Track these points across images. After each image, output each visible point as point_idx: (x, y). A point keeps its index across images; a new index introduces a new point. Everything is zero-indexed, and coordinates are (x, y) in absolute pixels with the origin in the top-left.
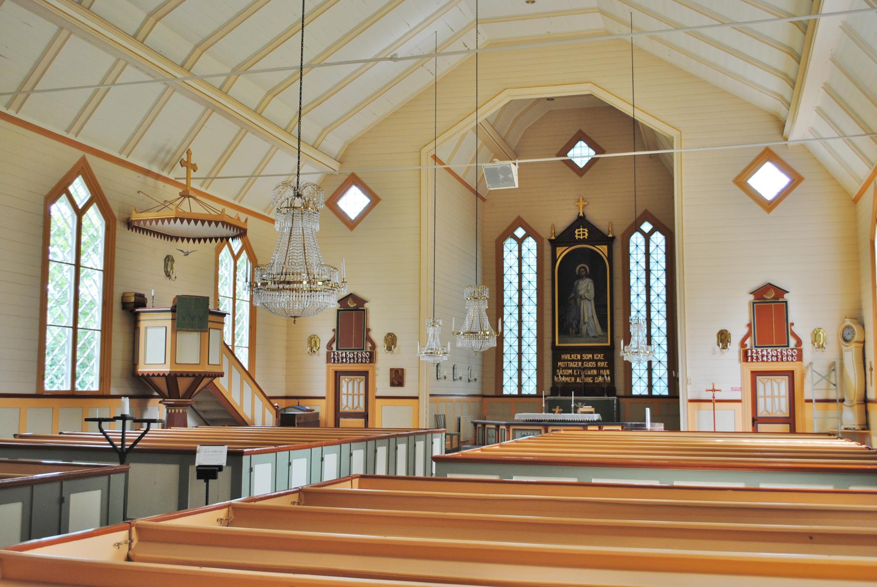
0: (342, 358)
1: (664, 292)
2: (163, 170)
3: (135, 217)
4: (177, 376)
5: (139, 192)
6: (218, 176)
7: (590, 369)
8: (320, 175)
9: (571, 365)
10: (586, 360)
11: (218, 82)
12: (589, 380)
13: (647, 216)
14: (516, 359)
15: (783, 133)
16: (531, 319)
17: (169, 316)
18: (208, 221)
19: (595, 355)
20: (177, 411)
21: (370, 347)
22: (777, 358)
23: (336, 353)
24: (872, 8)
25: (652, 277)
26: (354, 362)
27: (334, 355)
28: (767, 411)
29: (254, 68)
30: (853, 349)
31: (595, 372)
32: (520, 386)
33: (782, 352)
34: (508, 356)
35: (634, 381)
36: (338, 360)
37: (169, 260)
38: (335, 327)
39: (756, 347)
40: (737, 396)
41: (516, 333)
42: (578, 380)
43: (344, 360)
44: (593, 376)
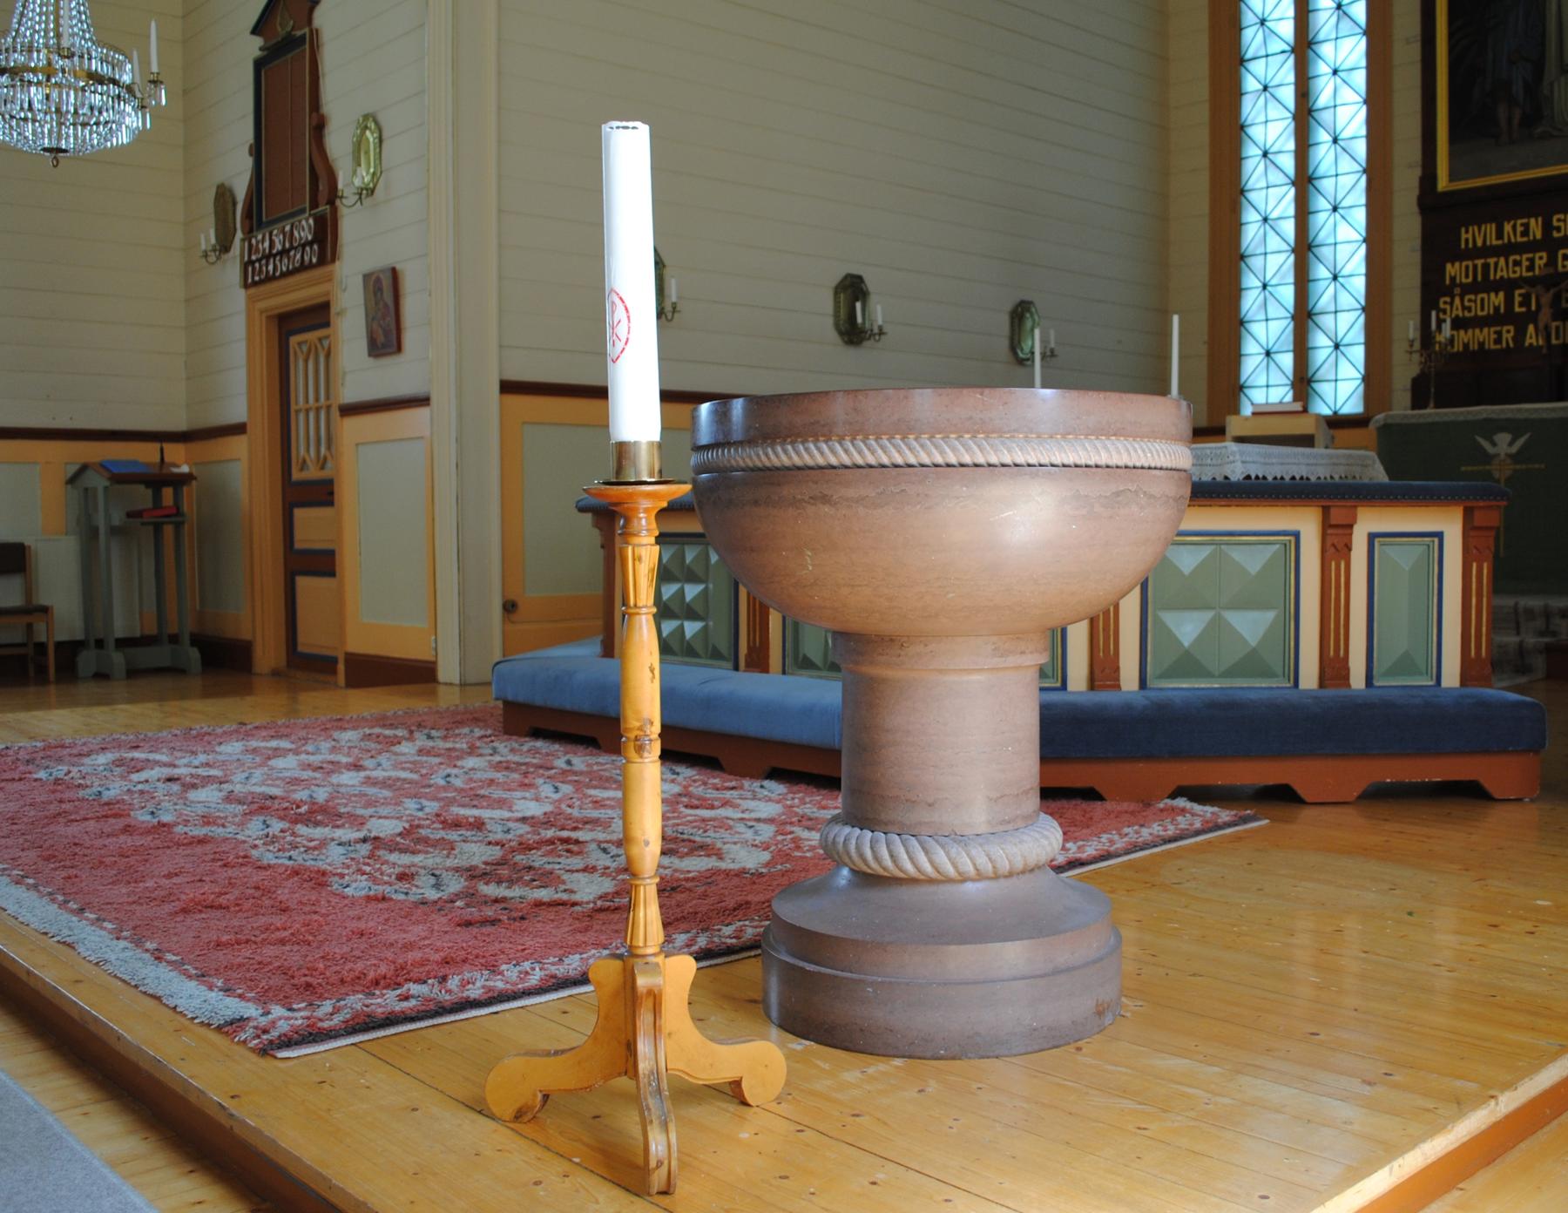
9: (1502, 269)
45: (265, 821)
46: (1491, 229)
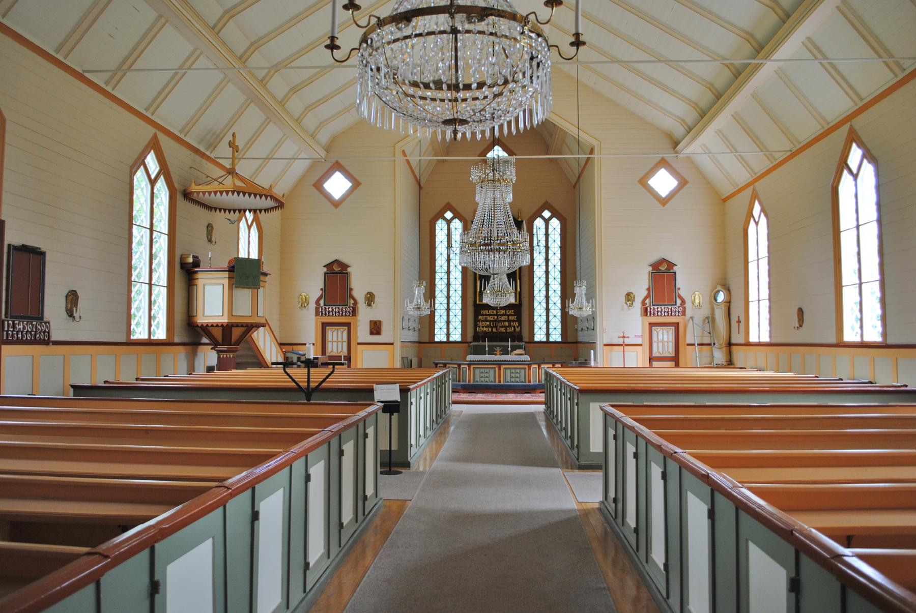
0: (329, 312)
1: (559, 264)
2: (207, 149)
3: (194, 188)
4: (234, 326)
5: (191, 167)
6: (244, 157)
7: (504, 321)
8: (310, 160)
9: (489, 318)
10: (500, 315)
11: (261, 74)
12: (503, 330)
13: (546, 206)
14: (445, 314)
15: (676, 147)
16: (457, 283)
17: (226, 275)
18: (254, 194)
19: (507, 311)
20: (228, 356)
21: (353, 304)
22: (339, 314)
23: (324, 308)
24: (815, 59)
25: (550, 252)
26: (339, 316)
27: (322, 309)
28: (659, 352)
29: (293, 64)
30: (723, 307)
31: (507, 324)
32: (448, 335)
33: (671, 309)
34: (439, 311)
35: (536, 330)
36: (325, 314)
37: (210, 227)
38: (322, 287)
39: (653, 305)
40: (639, 341)
41: (446, 293)
42: (494, 330)
43: (331, 314)
44: (506, 327)
45: (498, 118)
46: (487, 311)
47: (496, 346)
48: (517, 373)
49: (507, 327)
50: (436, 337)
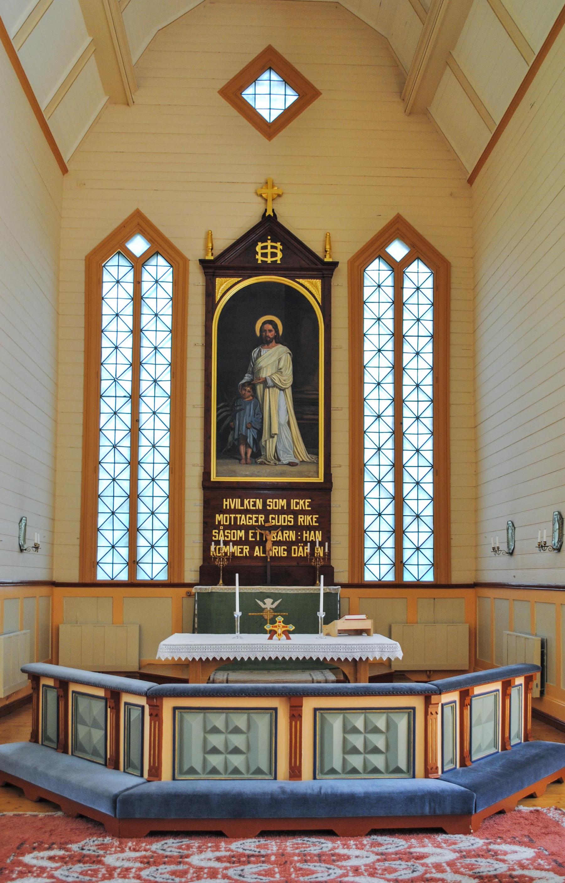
9: (243, 520)
10: (273, 512)
12: (280, 551)
19: (293, 502)
31: (292, 535)
42: (258, 552)
44: (289, 544)
46: (238, 501)
47: (263, 596)
48: (237, 731)
49: (292, 543)
50: (99, 570)
